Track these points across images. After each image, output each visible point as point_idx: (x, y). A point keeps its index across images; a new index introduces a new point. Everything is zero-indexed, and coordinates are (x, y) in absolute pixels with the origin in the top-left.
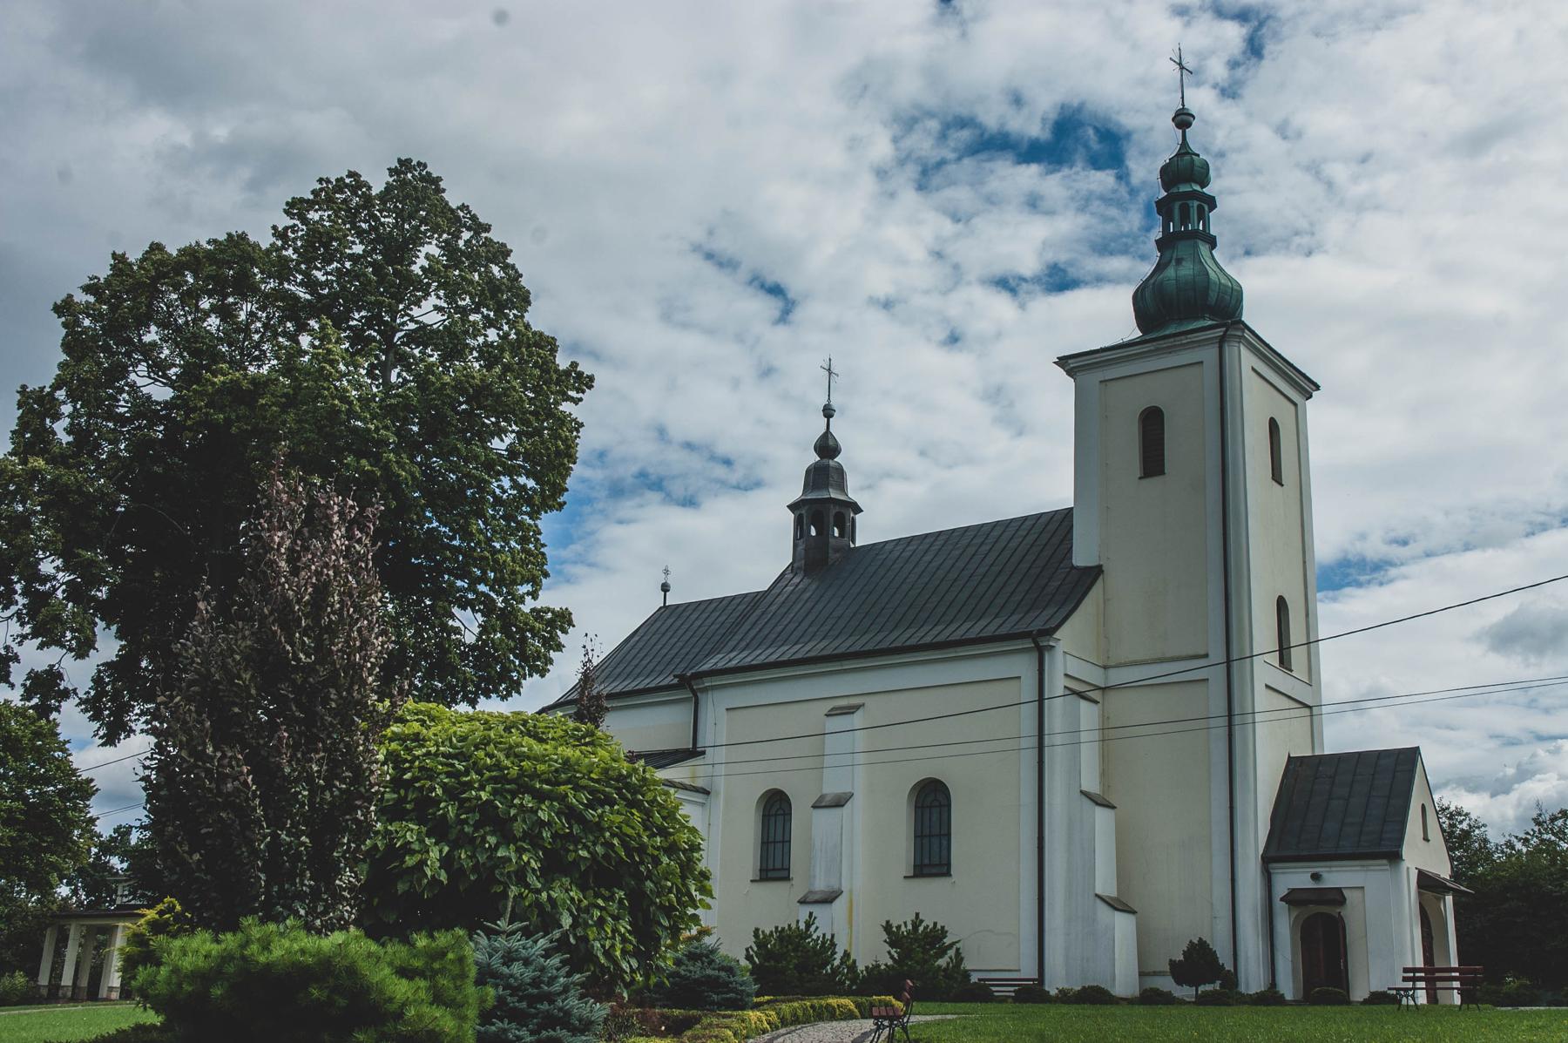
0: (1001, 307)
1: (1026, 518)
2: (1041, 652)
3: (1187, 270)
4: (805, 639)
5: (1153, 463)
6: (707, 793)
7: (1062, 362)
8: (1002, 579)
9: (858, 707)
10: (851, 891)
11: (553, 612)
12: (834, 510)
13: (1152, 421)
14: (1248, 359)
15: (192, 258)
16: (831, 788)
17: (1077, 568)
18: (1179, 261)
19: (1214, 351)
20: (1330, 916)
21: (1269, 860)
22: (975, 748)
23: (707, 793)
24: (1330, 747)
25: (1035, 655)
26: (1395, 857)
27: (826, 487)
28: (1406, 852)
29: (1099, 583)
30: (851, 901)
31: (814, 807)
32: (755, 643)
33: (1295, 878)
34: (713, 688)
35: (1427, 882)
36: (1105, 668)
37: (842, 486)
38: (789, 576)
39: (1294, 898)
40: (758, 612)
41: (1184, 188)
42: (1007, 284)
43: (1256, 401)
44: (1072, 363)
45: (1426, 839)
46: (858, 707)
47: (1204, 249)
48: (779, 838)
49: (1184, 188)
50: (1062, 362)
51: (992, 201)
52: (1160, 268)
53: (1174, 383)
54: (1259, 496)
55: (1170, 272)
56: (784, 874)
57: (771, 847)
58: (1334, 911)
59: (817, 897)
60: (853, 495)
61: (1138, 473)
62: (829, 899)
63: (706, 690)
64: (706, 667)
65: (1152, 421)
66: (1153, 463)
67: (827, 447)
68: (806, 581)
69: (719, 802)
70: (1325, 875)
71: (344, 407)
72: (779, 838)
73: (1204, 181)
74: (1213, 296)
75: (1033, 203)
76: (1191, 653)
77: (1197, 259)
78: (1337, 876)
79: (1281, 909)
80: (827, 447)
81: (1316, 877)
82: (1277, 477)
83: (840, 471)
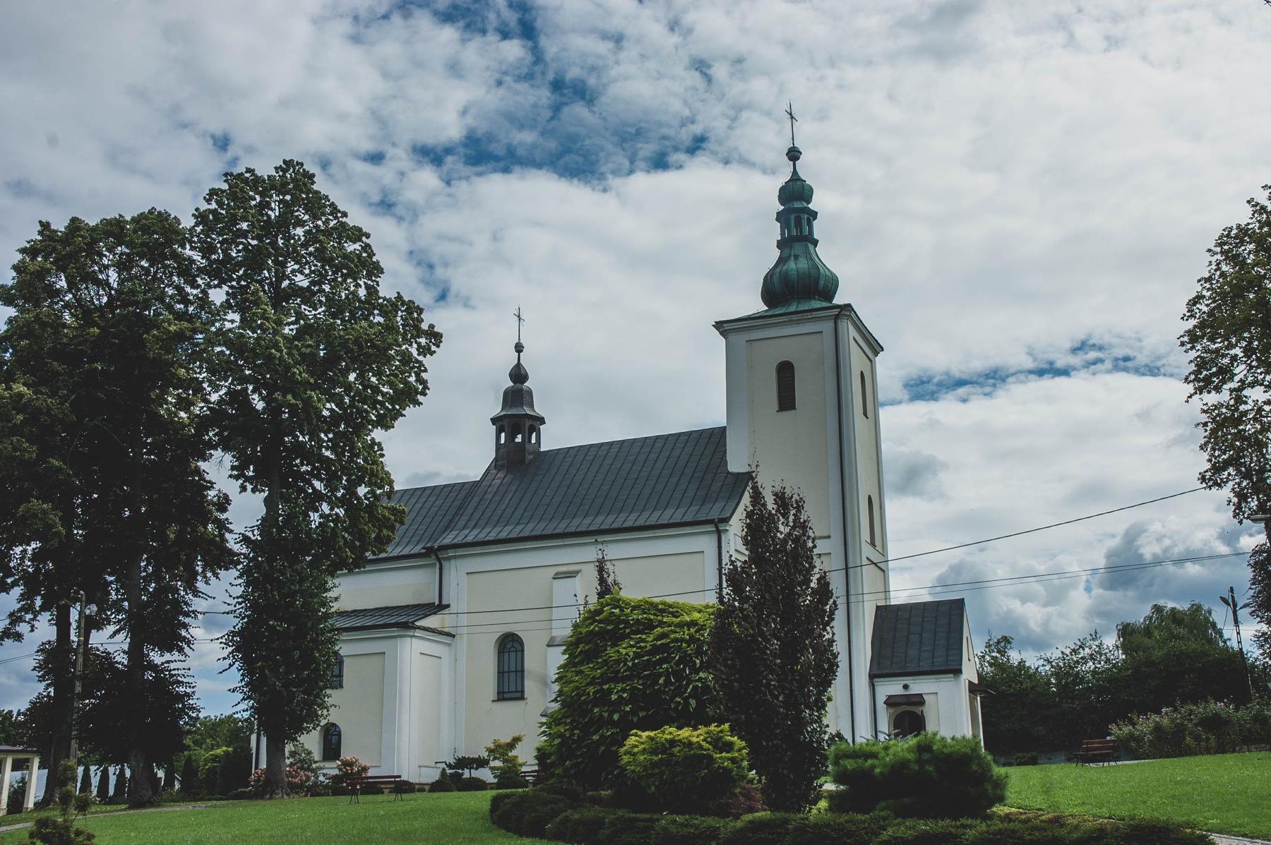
0: (428, 178)
1: (680, 434)
2: (719, 533)
3: (803, 264)
4: (525, 520)
5: (786, 401)
6: (454, 636)
7: (719, 325)
8: (674, 480)
12: (528, 423)
13: (786, 371)
14: (853, 332)
15: (114, 229)
17: (732, 474)
18: (796, 257)
19: (831, 324)
20: (915, 713)
21: (872, 677)
22: (479, 629)
24: (893, 602)
25: (715, 537)
26: (957, 672)
27: (521, 405)
31: (548, 646)
32: (482, 523)
33: (892, 688)
34: (455, 557)
37: (531, 406)
38: (494, 472)
39: (891, 702)
40: (476, 499)
41: (797, 205)
42: (431, 155)
43: (856, 359)
44: (726, 327)
46: (578, 572)
47: (811, 247)
49: (797, 205)
50: (719, 325)
51: (418, 64)
52: (782, 261)
53: (799, 342)
54: (860, 425)
55: (792, 265)
56: (519, 695)
57: (506, 675)
58: (917, 710)
60: (539, 409)
61: (792, 412)
63: (449, 559)
64: (447, 541)
65: (786, 371)
66: (786, 401)
67: (519, 375)
68: (509, 477)
69: (462, 643)
70: (911, 686)
71: (278, 355)
73: (809, 201)
74: (822, 282)
75: (455, 69)
77: (809, 257)
78: (919, 686)
80: (519, 375)
81: (906, 687)
82: (865, 414)
83: (530, 393)
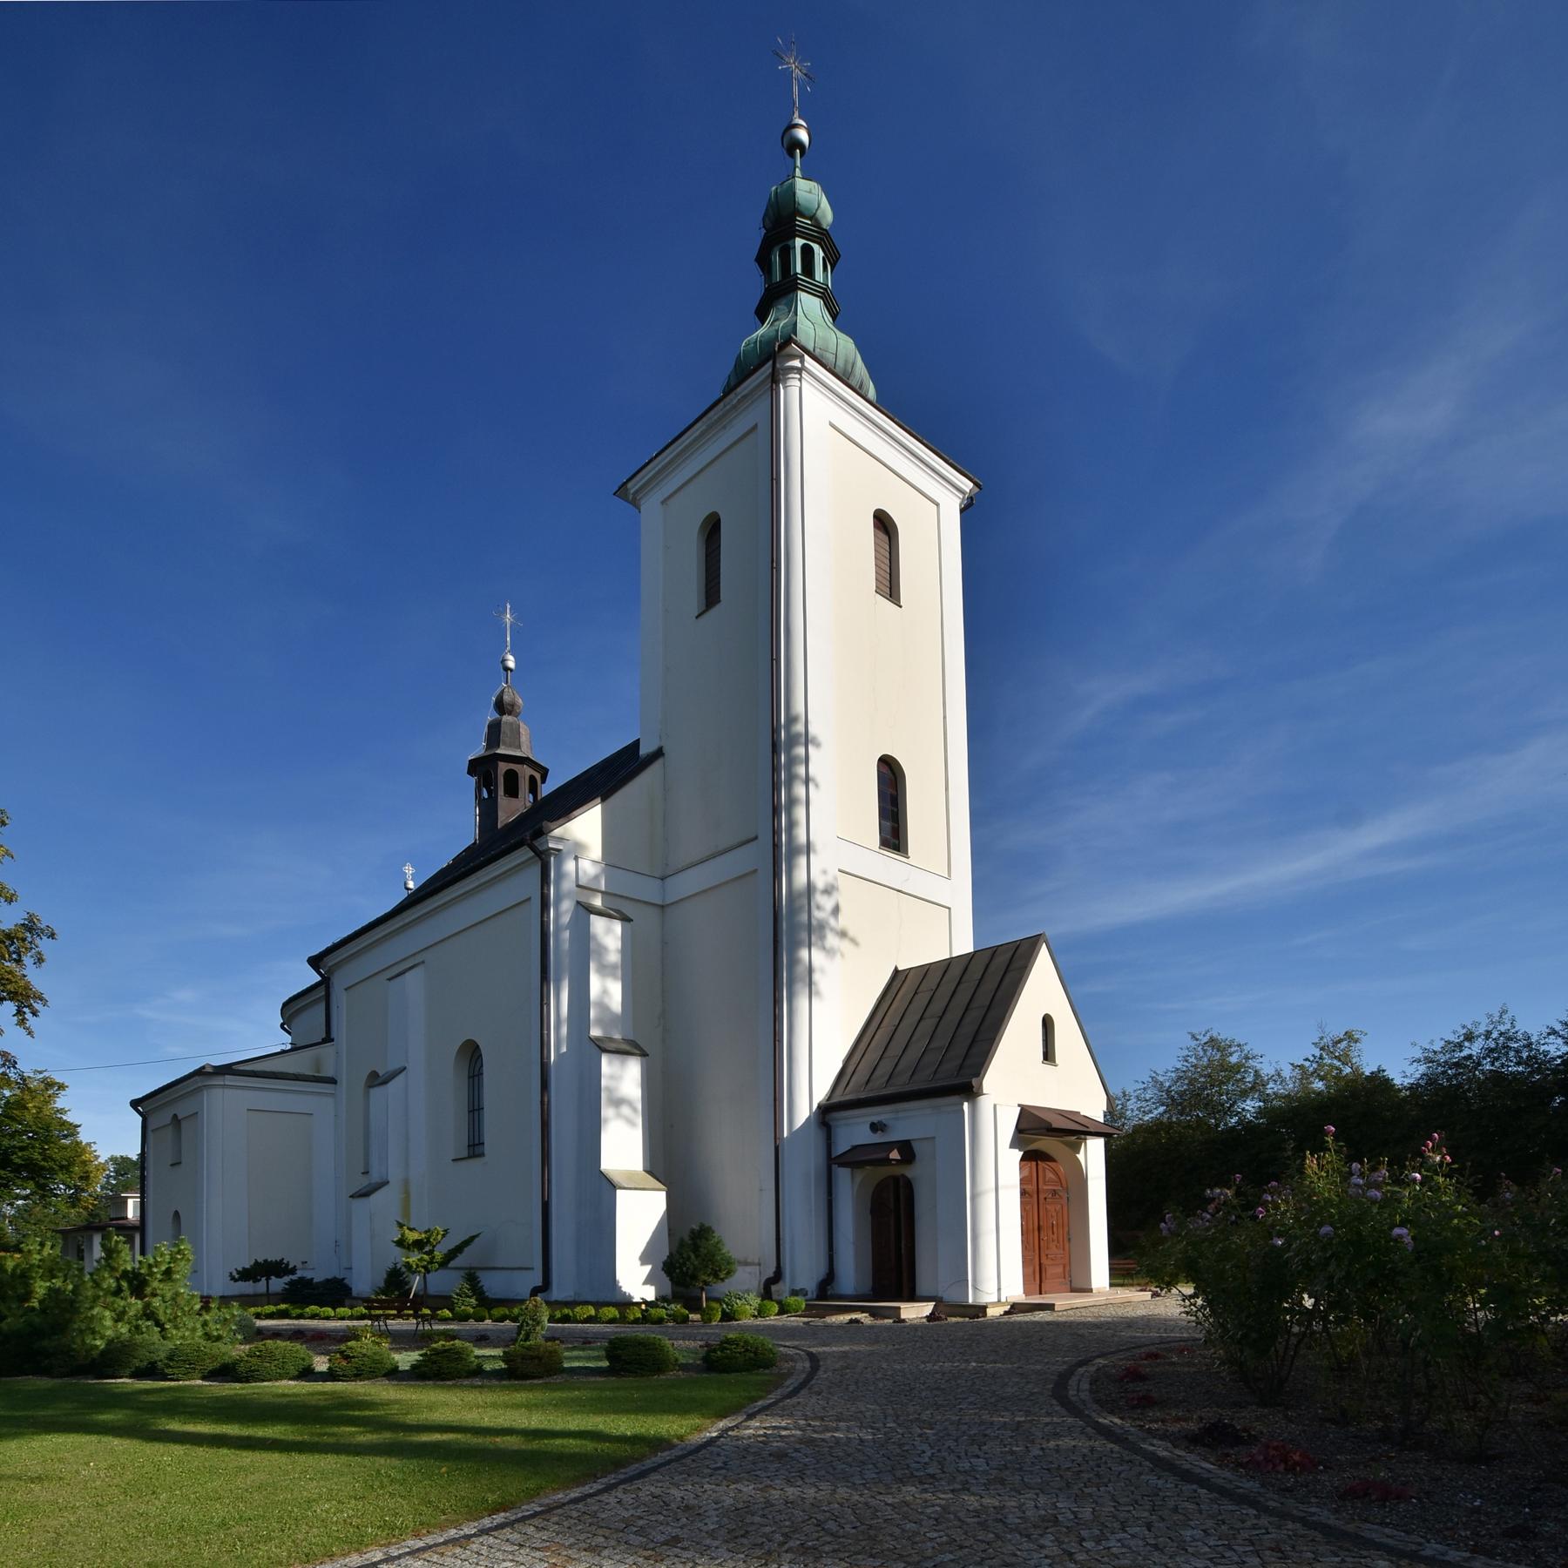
30: (407, 1193)
39: (856, 1159)
45: (1048, 1055)
81: (875, 1127)
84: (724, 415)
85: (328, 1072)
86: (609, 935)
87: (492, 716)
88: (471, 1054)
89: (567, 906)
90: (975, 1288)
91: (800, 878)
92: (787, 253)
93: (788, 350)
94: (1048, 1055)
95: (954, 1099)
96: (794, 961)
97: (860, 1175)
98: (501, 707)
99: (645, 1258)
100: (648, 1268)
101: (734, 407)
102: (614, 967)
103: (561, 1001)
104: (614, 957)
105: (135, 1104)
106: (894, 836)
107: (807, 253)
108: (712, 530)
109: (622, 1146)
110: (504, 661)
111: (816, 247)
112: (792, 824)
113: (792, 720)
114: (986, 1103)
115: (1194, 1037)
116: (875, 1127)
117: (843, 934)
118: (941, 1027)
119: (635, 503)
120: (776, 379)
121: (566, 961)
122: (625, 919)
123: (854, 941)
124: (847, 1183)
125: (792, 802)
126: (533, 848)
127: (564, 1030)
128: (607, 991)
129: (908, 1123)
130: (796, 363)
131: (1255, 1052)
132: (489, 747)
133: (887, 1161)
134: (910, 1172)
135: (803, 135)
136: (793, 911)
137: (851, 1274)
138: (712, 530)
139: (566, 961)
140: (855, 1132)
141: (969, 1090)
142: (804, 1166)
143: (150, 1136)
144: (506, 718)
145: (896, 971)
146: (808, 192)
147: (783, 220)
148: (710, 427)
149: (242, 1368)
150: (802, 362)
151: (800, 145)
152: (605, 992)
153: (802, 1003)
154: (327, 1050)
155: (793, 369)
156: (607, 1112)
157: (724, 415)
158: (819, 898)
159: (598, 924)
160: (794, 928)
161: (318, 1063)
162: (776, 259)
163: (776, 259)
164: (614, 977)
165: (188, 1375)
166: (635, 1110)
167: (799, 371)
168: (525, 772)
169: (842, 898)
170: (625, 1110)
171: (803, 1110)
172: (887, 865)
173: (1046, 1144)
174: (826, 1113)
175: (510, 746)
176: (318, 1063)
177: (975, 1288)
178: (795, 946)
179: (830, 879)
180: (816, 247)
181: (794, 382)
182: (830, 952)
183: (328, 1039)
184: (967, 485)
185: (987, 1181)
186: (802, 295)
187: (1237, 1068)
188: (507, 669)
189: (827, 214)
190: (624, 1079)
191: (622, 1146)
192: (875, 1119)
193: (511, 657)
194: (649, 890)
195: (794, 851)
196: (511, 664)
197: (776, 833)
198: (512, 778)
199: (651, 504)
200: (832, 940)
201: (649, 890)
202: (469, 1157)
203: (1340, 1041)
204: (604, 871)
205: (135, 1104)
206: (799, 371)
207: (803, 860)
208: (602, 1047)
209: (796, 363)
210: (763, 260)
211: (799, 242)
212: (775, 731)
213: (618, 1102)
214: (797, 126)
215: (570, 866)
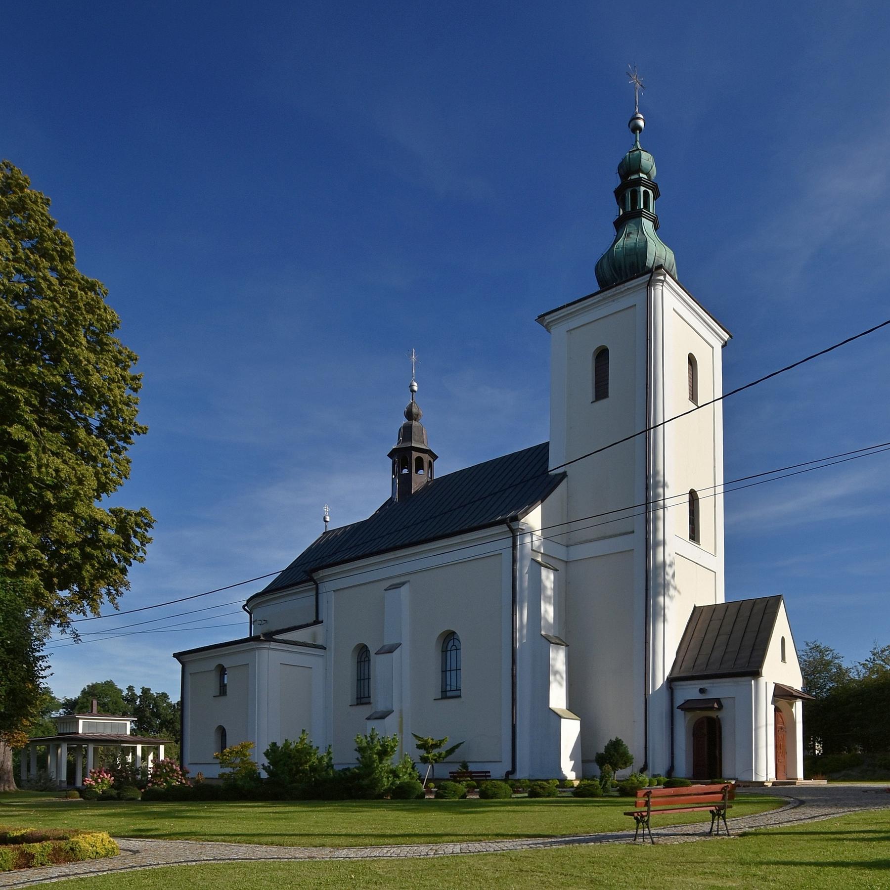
6: (325, 649)
9: (403, 584)
10: (401, 711)
11: (736, 779)
16: (388, 641)
18: (628, 235)
23: (325, 649)
28: (766, 669)
29: (565, 480)
30: (401, 717)
35: (782, 694)
36: (567, 546)
39: (688, 706)
45: (783, 659)
48: (454, 667)
59: (377, 716)
62: (383, 716)
66: (601, 391)
72: (454, 667)
76: (623, 531)
79: (679, 714)
81: (702, 691)
84: (615, 295)
85: (320, 642)
86: (548, 579)
87: (405, 421)
88: (449, 641)
89: (527, 563)
90: (756, 774)
91: (660, 558)
92: (635, 194)
93: (659, 271)
94: (783, 659)
95: (748, 678)
96: (656, 603)
97: (690, 715)
98: (410, 415)
99: (572, 757)
100: (573, 762)
101: (622, 292)
102: (550, 598)
103: (523, 616)
104: (550, 592)
105: (177, 656)
106: (694, 535)
107: (646, 194)
108: (602, 356)
109: (558, 698)
110: (411, 386)
111: (650, 192)
112: (656, 530)
113: (656, 473)
114: (762, 680)
115: (807, 645)
116: (702, 691)
117: (675, 588)
118: (730, 640)
119: (547, 328)
120: (650, 284)
121: (526, 593)
122: (555, 570)
123: (679, 591)
124: (683, 723)
125: (656, 519)
126: (509, 526)
127: (525, 631)
128: (548, 611)
129: (719, 689)
130: (662, 278)
131: (840, 655)
132: (404, 440)
133: (712, 708)
134: (720, 714)
135: (641, 123)
136: (656, 576)
137: (683, 767)
138: (602, 356)
139: (526, 593)
140: (689, 692)
141: (756, 674)
142: (659, 709)
143: (188, 678)
144: (414, 423)
145: (695, 607)
146: (647, 159)
147: (629, 170)
148: (604, 299)
149: (490, 792)
150: (665, 277)
151: (640, 128)
152: (546, 611)
153: (660, 626)
154: (318, 628)
155: (660, 280)
156: (552, 678)
157: (615, 295)
158: (668, 569)
159: (544, 572)
160: (657, 585)
161: (314, 636)
162: (628, 195)
163: (628, 195)
164: (550, 603)
165: (454, 796)
166: (562, 678)
167: (663, 281)
168: (426, 457)
169: (676, 567)
170: (558, 677)
171: (660, 681)
172: (689, 548)
173: (782, 703)
174: (671, 681)
175: (417, 441)
176: (314, 636)
177: (756, 774)
178: (656, 595)
179: (671, 558)
180: (650, 192)
181: (659, 287)
182: (671, 598)
183: (317, 622)
184: (726, 337)
185: (762, 722)
186: (644, 220)
187: (829, 663)
188: (413, 391)
189: (654, 172)
190: (558, 659)
191: (558, 698)
192: (702, 687)
193: (415, 384)
194: (560, 552)
195: (656, 544)
196: (416, 388)
197: (647, 533)
198: (419, 461)
199: (559, 331)
200: (672, 592)
201: (560, 552)
202: (442, 698)
203: (885, 650)
204: (542, 543)
205: (177, 656)
206: (663, 281)
207: (661, 549)
208: (548, 640)
209: (662, 278)
210: (619, 194)
211: (642, 189)
212: (647, 478)
213: (556, 673)
214: (639, 118)
215: (528, 540)
